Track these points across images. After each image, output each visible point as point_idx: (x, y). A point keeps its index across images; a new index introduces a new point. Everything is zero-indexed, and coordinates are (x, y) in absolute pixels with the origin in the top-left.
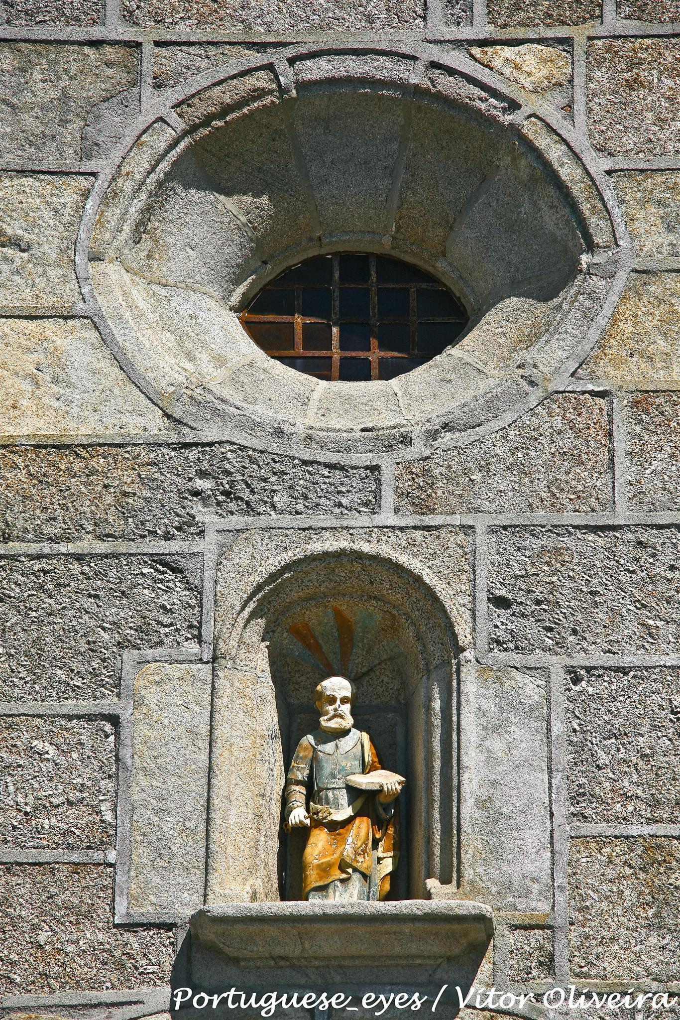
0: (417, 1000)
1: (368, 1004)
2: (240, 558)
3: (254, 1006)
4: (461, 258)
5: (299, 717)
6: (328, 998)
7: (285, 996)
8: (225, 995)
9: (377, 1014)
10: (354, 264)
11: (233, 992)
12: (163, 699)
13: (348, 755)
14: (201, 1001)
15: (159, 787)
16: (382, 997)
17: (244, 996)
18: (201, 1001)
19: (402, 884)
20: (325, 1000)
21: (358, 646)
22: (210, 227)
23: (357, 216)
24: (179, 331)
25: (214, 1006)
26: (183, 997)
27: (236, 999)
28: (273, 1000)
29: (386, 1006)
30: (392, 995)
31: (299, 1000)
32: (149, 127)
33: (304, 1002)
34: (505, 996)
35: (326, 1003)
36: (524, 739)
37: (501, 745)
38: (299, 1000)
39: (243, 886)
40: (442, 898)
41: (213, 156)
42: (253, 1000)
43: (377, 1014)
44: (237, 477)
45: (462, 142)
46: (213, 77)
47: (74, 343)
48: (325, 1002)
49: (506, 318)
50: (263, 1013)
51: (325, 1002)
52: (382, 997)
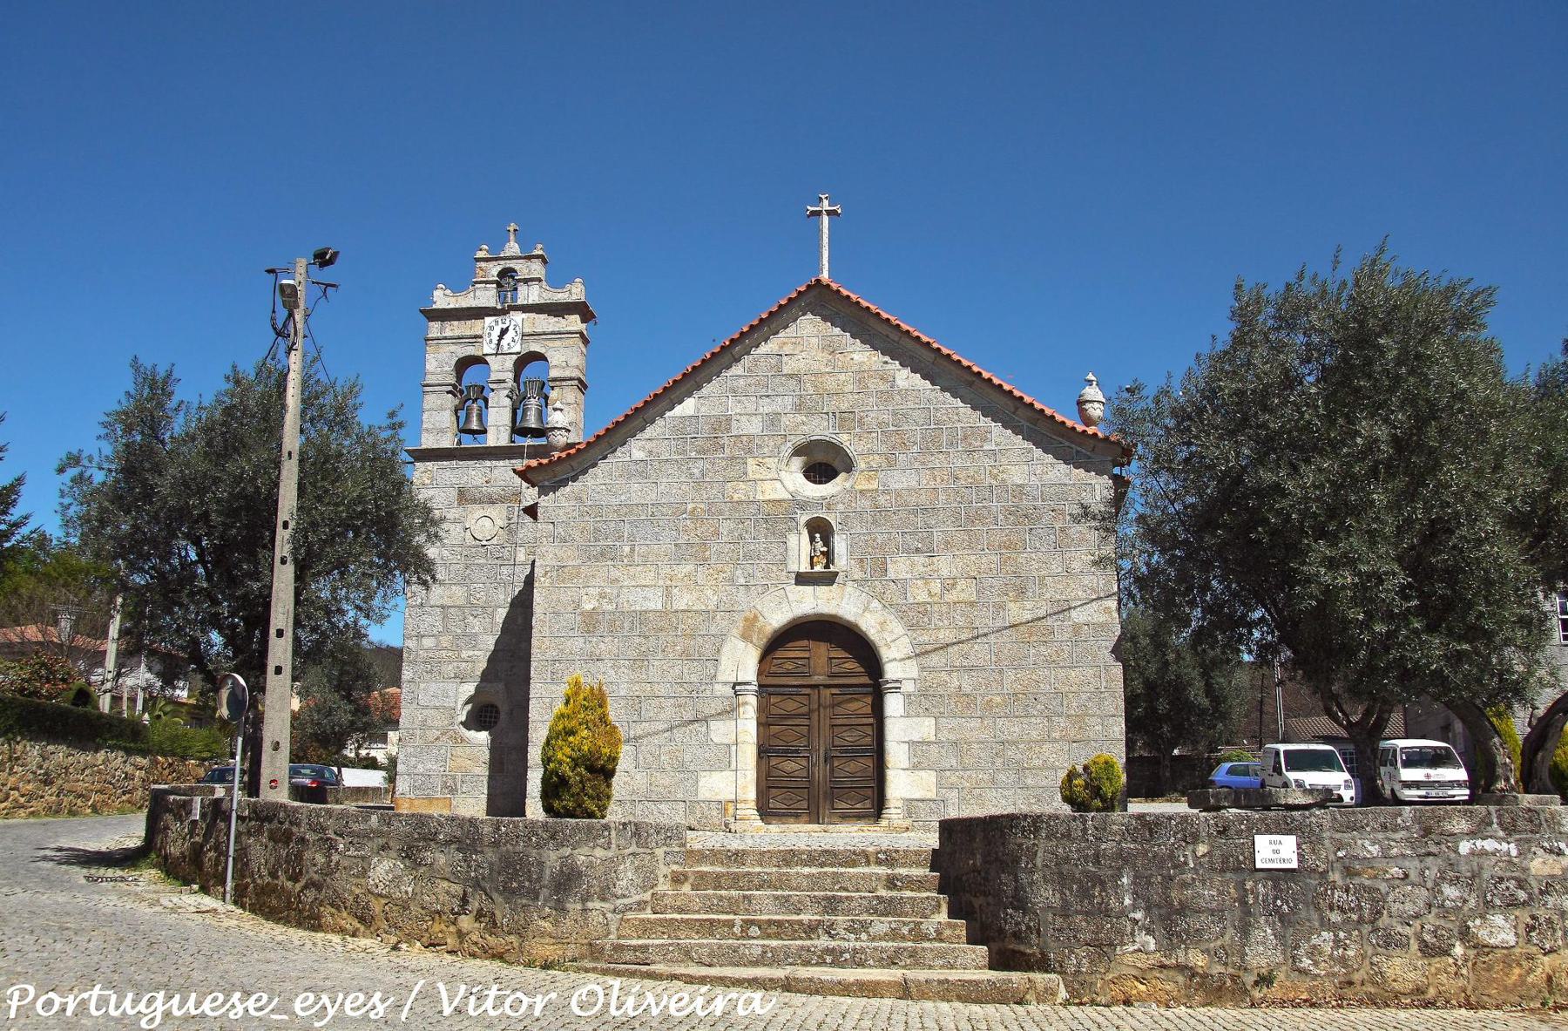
0: (378, 1004)
1: (303, 1009)
2: (803, 518)
3: (130, 1012)
4: (836, 464)
5: (812, 539)
6: (241, 1001)
7: (177, 997)
8: (85, 995)
9: (317, 1025)
10: (820, 464)
11: (97, 991)
12: (792, 539)
13: (820, 546)
14: (48, 1004)
15: (793, 553)
16: (325, 999)
17: (114, 998)
18: (48, 1004)
19: (827, 566)
20: (237, 1004)
21: (820, 530)
22: (798, 463)
23: (820, 457)
24: (794, 481)
25: (69, 1013)
26: (21, 998)
27: (103, 1002)
28: (158, 1003)
29: (331, 1012)
30: (341, 996)
31: (198, 1004)
32: (788, 449)
33: (206, 1007)
34: (512, 997)
35: (240, 1009)
36: (844, 544)
37: (840, 544)
38: (198, 1004)
39: (805, 567)
40: (832, 569)
41: (798, 452)
42: (127, 1003)
43: (317, 1025)
44: (803, 505)
45: (836, 449)
46: (799, 440)
47: (778, 484)
48: (238, 1006)
49: (842, 475)
50: (143, 1024)
51: (238, 1006)
52: (325, 999)
